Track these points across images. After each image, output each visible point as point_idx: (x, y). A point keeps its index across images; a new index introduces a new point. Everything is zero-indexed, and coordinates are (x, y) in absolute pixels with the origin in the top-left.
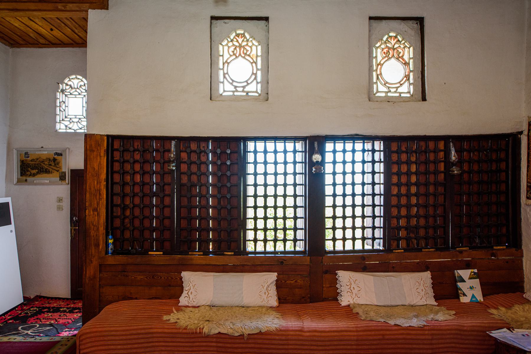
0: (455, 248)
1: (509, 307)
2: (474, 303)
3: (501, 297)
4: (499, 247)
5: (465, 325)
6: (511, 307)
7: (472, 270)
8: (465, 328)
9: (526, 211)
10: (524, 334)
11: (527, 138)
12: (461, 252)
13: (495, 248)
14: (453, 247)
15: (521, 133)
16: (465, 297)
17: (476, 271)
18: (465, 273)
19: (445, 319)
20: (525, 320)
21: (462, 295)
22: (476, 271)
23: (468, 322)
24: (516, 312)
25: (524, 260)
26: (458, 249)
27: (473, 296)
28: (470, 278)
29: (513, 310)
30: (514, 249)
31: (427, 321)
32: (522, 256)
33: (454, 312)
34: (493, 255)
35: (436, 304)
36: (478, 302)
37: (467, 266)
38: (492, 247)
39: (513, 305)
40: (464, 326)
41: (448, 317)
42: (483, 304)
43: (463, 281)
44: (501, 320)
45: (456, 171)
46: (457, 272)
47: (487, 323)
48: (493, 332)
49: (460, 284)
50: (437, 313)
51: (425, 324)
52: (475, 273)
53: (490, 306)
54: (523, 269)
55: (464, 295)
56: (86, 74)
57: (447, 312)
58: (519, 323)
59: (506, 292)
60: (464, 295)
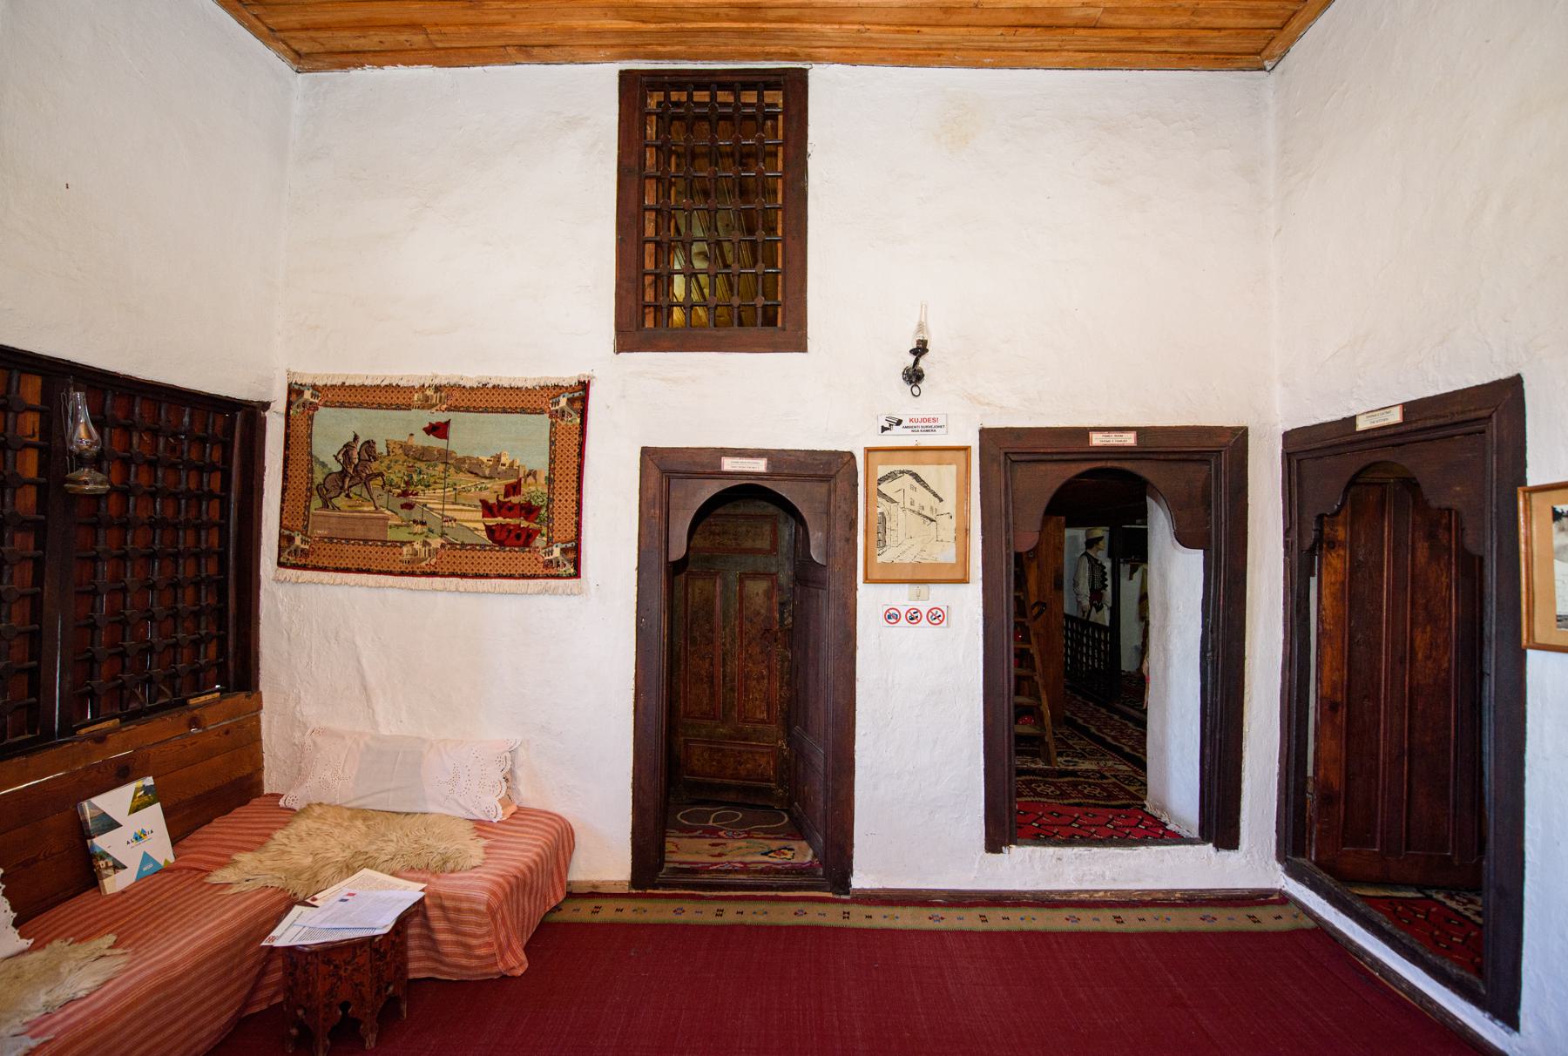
0: (73, 732)
1: (258, 843)
2: (155, 876)
3: (220, 828)
4: (203, 698)
5: (177, 958)
6: (262, 844)
7: (139, 784)
8: (180, 969)
9: (274, 595)
10: (342, 895)
11: (283, 421)
12: (100, 739)
13: (192, 702)
14: (68, 729)
15: (266, 406)
16: (122, 872)
17: (149, 781)
18: (115, 801)
19: (100, 979)
20: (315, 862)
21: (110, 871)
22: (149, 781)
23: (185, 942)
24: (284, 852)
25: (264, 716)
26: (83, 731)
27: (146, 858)
28: (134, 809)
29: (272, 846)
30: (243, 694)
31: (33, 1028)
32: (260, 707)
33: (111, 938)
34: (194, 722)
35: (25, 943)
36: (162, 871)
37: (121, 775)
38: (184, 702)
39: (269, 836)
40: (174, 965)
41: (105, 968)
42: (180, 869)
43: (113, 825)
44: (259, 891)
45: (90, 481)
46: (94, 807)
47: (234, 917)
48: (274, 934)
49: (101, 842)
50: (52, 974)
51: (33, 1043)
52: (147, 789)
53: (203, 866)
54: (260, 740)
55: (118, 866)
56: (187, 833)
57: (84, 950)
58: (306, 876)
59: (227, 811)
60: (118, 866)
